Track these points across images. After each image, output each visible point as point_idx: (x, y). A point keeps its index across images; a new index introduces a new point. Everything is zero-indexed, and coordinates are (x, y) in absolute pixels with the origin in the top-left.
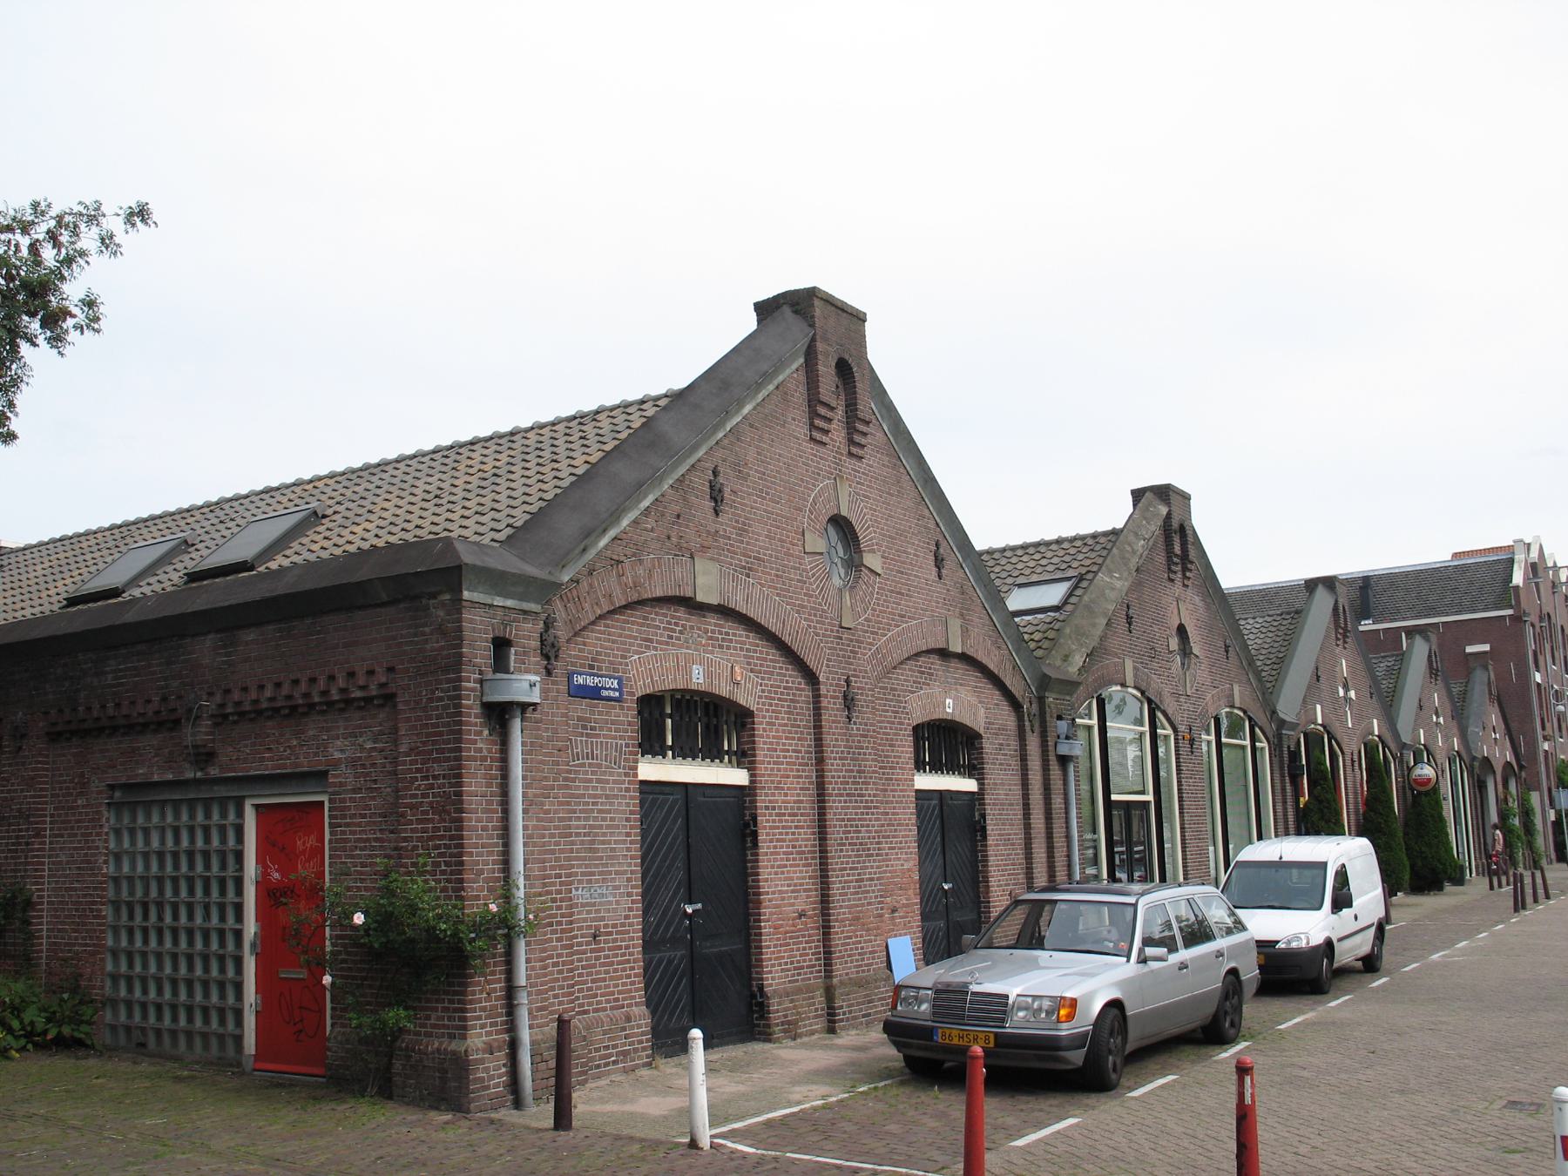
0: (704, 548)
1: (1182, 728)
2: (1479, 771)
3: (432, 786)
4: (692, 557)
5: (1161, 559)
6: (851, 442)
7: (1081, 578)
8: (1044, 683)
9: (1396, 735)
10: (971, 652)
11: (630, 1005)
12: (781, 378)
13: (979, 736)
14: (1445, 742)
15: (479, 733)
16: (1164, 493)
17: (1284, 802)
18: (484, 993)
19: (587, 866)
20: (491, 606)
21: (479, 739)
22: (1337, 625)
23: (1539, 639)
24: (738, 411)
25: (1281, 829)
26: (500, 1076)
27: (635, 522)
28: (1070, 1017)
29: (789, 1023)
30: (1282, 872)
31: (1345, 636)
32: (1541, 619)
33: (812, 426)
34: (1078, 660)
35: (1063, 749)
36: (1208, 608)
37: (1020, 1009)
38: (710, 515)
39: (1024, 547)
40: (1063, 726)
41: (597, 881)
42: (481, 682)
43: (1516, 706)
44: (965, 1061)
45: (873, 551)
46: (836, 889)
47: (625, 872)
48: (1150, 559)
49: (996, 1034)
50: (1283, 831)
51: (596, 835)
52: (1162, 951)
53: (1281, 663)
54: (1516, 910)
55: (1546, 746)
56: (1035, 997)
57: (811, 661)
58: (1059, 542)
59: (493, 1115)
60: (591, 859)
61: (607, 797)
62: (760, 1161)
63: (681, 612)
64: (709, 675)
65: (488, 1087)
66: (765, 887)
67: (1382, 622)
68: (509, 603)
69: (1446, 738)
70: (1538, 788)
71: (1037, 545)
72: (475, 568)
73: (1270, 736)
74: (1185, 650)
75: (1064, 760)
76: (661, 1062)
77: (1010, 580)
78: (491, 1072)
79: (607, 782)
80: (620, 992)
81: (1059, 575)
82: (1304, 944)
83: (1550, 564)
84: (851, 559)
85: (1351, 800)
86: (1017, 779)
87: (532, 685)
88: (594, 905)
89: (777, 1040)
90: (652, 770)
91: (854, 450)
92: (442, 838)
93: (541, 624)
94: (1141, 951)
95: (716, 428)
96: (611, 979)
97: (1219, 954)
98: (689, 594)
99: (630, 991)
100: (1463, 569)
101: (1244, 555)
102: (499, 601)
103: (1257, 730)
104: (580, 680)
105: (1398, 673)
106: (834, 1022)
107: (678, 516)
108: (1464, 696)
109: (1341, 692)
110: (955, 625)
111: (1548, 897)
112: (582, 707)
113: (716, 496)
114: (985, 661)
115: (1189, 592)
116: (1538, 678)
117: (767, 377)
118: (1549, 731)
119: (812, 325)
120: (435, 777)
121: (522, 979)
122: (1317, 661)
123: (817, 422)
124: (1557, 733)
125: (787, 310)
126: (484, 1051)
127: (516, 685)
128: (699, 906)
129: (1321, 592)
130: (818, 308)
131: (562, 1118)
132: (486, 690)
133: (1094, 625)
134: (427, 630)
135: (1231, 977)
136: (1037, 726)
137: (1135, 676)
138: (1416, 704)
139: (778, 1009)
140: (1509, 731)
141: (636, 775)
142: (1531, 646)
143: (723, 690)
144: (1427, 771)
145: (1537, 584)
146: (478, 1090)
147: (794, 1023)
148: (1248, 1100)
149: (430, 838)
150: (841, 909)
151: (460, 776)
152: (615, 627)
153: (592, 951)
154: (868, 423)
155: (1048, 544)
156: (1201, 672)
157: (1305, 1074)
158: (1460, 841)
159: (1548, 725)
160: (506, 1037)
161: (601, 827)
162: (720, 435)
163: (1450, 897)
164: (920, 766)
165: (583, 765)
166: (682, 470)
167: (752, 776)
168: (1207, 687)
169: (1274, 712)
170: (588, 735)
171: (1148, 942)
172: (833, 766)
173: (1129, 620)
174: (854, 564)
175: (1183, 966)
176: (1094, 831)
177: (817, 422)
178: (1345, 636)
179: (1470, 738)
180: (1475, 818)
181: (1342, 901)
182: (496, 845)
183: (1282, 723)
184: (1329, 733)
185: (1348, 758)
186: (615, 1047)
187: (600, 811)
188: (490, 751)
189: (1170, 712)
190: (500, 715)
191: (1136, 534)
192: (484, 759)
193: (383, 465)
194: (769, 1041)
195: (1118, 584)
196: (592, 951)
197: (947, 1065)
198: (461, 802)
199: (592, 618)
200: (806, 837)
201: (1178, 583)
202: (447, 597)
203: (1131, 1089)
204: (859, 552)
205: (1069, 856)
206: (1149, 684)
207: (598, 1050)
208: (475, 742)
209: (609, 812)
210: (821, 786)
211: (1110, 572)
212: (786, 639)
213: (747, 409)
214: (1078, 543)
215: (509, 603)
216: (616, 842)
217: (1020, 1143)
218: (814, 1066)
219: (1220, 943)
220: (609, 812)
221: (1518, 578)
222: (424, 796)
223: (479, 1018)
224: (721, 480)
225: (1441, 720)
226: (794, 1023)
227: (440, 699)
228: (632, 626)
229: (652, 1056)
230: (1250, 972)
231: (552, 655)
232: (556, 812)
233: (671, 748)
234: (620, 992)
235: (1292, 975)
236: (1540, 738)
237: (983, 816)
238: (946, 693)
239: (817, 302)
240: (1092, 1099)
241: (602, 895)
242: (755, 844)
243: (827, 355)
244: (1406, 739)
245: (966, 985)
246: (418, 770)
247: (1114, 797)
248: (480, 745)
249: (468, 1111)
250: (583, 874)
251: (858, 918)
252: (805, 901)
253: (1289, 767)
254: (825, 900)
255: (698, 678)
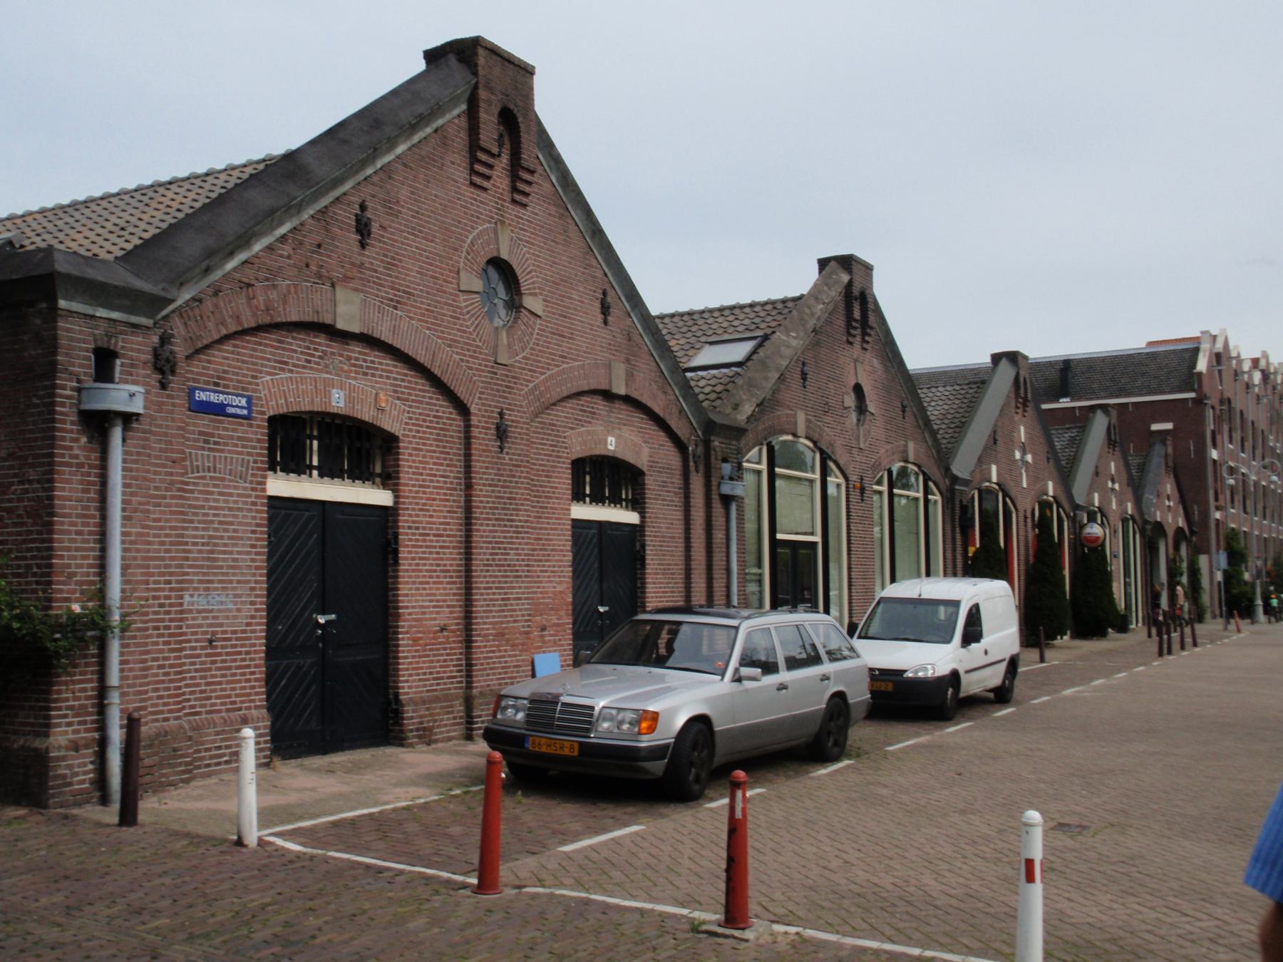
0: (347, 279)
1: (853, 478)
2: (1152, 534)
3: (26, 491)
4: (333, 286)
5: (840, 322)
6: (515, 189)
7: (766, 338)
8: (710, 428)
9: (1070, 497)
10: (635, 395)
11: (249, 708)
12: (440, 122)
13: (642, 473)
14: (1119, 504)
15: (76, 440)
16: (847, 262)
17: (954, 550)
18: (72, 692)
19: (204, 574)
20: (93, 317)
21: (73, 445)
22: (1017, 395)
23: (1218, 420)
24: (389, 150)
25: (950, 570)
26: (85, 773)
27: (270, 248)
28: (651, 729)
29: (424, 729)
30: (922, 609)
31: (1025, 405)
32: (1222, 402)
33: (473, 171)
34: (748, 409)
35: (727, 489)
36: (886, 370)
37: (605, 720)
38: (356, 249)
39: (721, 310)
40: (727, 468)
41: (217, 589)
42: (79, 390)
43: (1192, 480)
44: (566, 769)
45: (535, 295)
46: (479, 607)
47: (248, 582)
48: (829, 322)
49: (581, 744)
50: (951, 571)
51: (216, 545)
52: (757, 671)
53: (961, 427)
54: (1161, 654)
55: (1218, 515)
56: (620, 709)
57: (461, 392)
58: (752, 305)
59: (75, 811)
60: (209, 567)
61: (230, 509)
62: (299, 856)
63: (321, 339)
64: (350, 399)
65: (71, 784)
66: (404, 602)
67: (1079, 400)
68: (115, 315)
69: (1121, 503)
70: (1207, 552)
71: (732, 308)
72: (68, 277)
73: (944, 490)
74: (861, 409)
75: (727, 500)
76: (277, 762)
77: (703, 339)
78: (79, 771)
79: (231, 495)
80: (237, 695)
81: (748, 335)
82: (930, 674)
83: (1234, 354)
84: (512, 300)
85: (1022, 552)
86: (679, 515)
87: (132, 395)
88: (211, 611)
89: (411, 745)
90: (281, 486)
91: (478, 180)
92: (34, 541)
93: (156, 339)
94: (737, 670)
95: (364, 163)
96: (228, 682)
97: (825, 678)
98: (328, 321)
99: (249, 695)
100: (1153, 356)
101: (936, 331)
102: (101, 313)
103: (931, 484)
104: (201, 396)
105: (1077, 445)
106: (472, 729)
107: (319, 246)
108: (1143, 468)
109: (1018, 455)
110: (620, 370)
111: (1195, 644)
112: (204, 422)
113: (363, 229)
114: (650, 404)
115: (868, 355)
116: (1214, 454)
117: (422, 120)
118: (1221, 502)
119: (475, 74)
120: (30, 482)
121: (114, 678)
122: (995, 425)
123: (478, 167)
124: (1229, 505)
125: (452, 59)
126: (67, 749)
127: (113, 393)
128: (333, 617)
129: (1004, 363)
130: (482, 58)
131: (128, 816)
132: (84, 399)
133: (766, 379)
134: (26, 338)
135: (837, 700)
136: (701, 468)
137: (808, 427)
138: (1092, 469)
139: (412, 718)
140: (1183, 500)
141: (264, 490)
142: (1210, 426)
143: (366, 414)
144: (1095, 530)
145: (1220, 372)
146: (59, 786)
147: (430, 729)
148: (739, 815)
149: (24, 541)
150: (484, 624)
151: (52, 481)
152: (246, 348)
153: (208, 655)
154: (532, 172)
155: (742, 307)
156: (876, 428)
157: (885, 792)
158: (1124, 589)
159: (1221, 497)
160: (96, 735)
161: (222, 538)
162: (369, 171)
163: (1113, 641)
164: (578, 496)
165: (203, 478)
166: (325, 201)
167: (396, 497)
168: (879, 442)
169: (948, 469)
170: (210, 449)
171: (747, 661)
172: (482, 494)
173: (804, 376)
174: (514, 305)
175: (782, 687)
176: (759, 564)
177: (478, 167)
178: (1025, 405)
179: (1144, 506)
180: (1144, 570)
181: (973, 633)
182: (93, 549)
183: (955, 479)
184: (1003, 491)
185: (1021, 514)
186: (227, 747)
187: (221, 523)
188: (88, 458)
189: (841, 462)
190: (98, 424)
191: (817, 298)
192: (80, 465)
193: (87, 203)
194: (402, 745)
195: (794, 343)
196: (208, 655)
197: (551, 773)
198: (52, 506)
199: (216, 337)
200: (452, 558)
201: (857, 345)
202: (44, 305)
203: (712, 800)
204: (520, 294)
205: (728, 587)
206: (821, 435)
207: (209, 750)
208: (70, 448)
209: (231, 523)
210: (468, 509)
211: (787, 332)
212: (437, 371)
213: (401, 149)
214: (769, 307)
215: (115, 315)
216: (239, 553)
217: (568, 848)
218: (432, 769)
219: (827, 667)
220: (231, 523)
221: (1202, 365)
222: (20, 500)
223: (65, 716)
224: (369, 214)
225: (1117, 486)
226: (430, 729)
227: (37, 406)
228: (267, 347)
229: (270, 757)
230: (859, 695)
231: (167, 368)
232: (167, 520)
233: (380, 475)
234: (237, 695)
235: (904, 701)
236: (1212, 508)
237: (643, 546)
238: (609, 433)
239: (481, 51)
240: (669, 810)
241: (222, 603)
242: (396, 562)
243: (489, 102)
244: (1080, 500)
245: (557, 696)
246: (15, 475)
247: (779, 536)
248: (76, 452)
249: (46, 807)
250: (200, 582)
251: (503, 635)
252: (449, 615)
253: (959, 518)
254: (468, 616)
255: (338, 401)
